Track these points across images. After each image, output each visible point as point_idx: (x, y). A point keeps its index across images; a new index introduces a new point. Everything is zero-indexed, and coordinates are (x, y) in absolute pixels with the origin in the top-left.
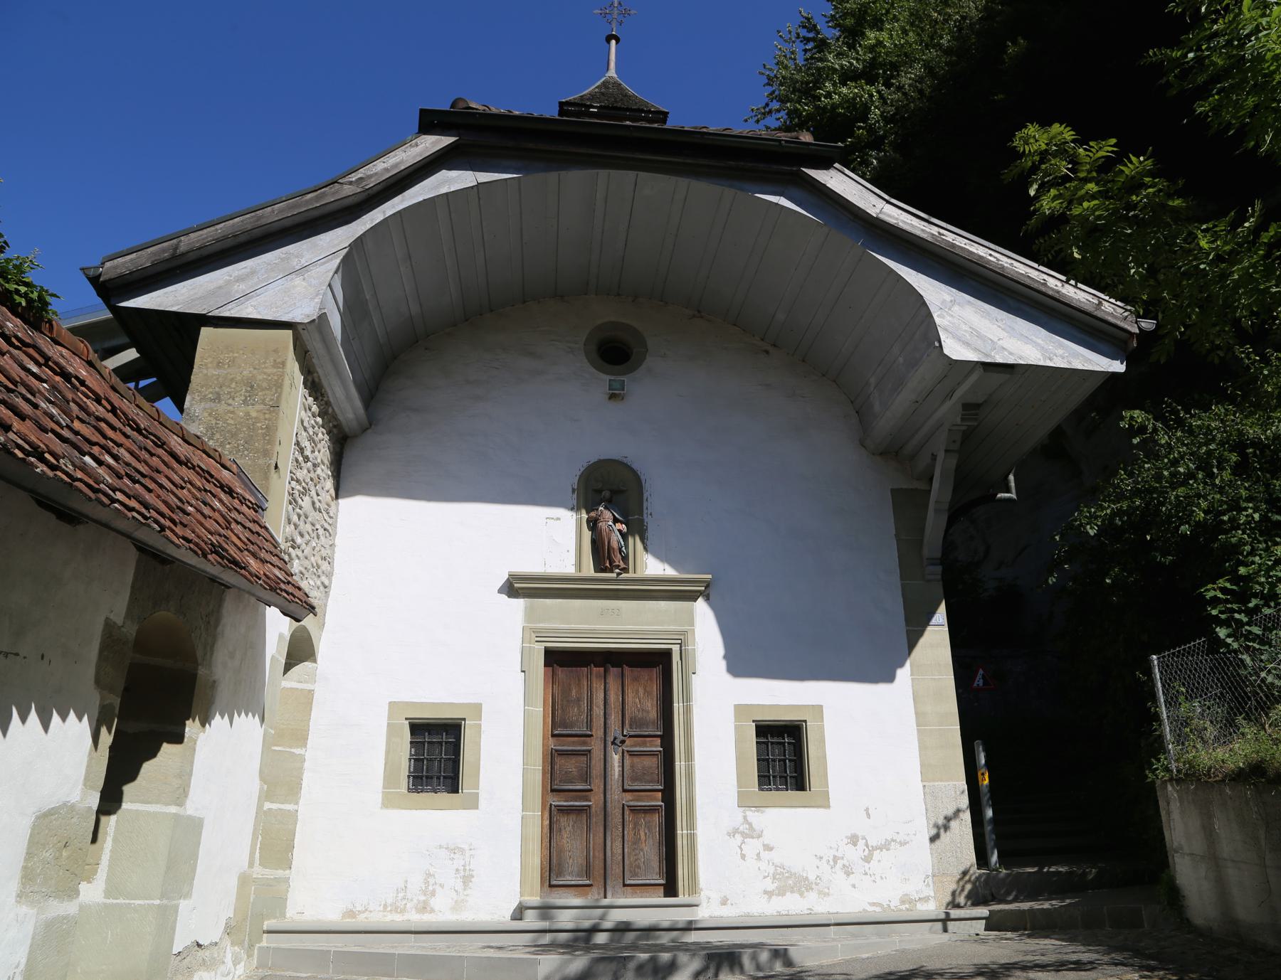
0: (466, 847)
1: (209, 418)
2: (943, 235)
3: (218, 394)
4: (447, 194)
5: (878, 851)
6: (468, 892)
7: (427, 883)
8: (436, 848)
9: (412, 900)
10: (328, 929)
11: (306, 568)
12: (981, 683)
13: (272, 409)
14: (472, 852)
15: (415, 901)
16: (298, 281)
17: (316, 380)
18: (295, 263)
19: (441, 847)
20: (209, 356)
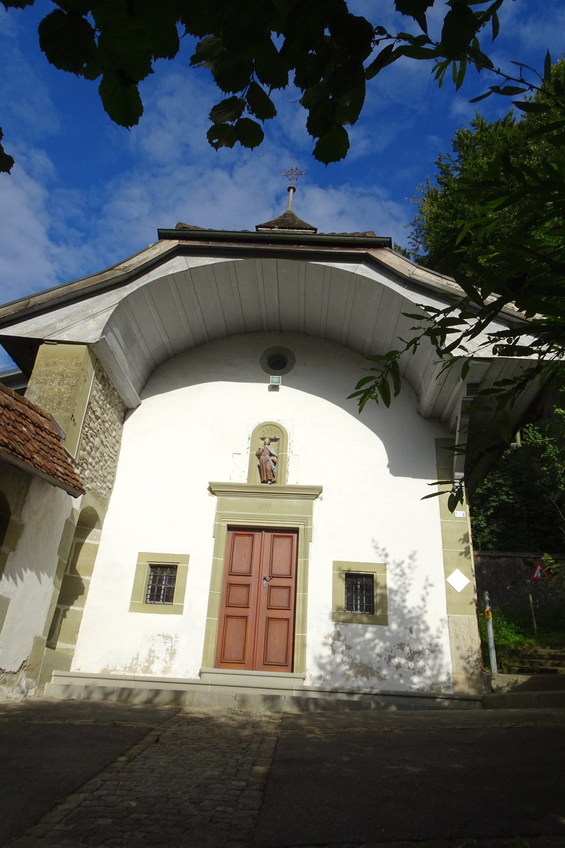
0: (174, 636)
1: (40, 392)
2: (450, 285)
3: (45, 380)
4: (172, 274)
5: (417, 655)
6: (173, 662)
7: (150, 656)
8: (157, 635)
9: (140, 665)
10: (94, 677)
11: (95, 476)
12: (539, 575)
13: (72, 387)
14: (177, 639)
15: (142, 666)
16: (91, 321)
17: (105, 375)
18: (90, 312)
19: (159, 635)
20: (43, 361)
